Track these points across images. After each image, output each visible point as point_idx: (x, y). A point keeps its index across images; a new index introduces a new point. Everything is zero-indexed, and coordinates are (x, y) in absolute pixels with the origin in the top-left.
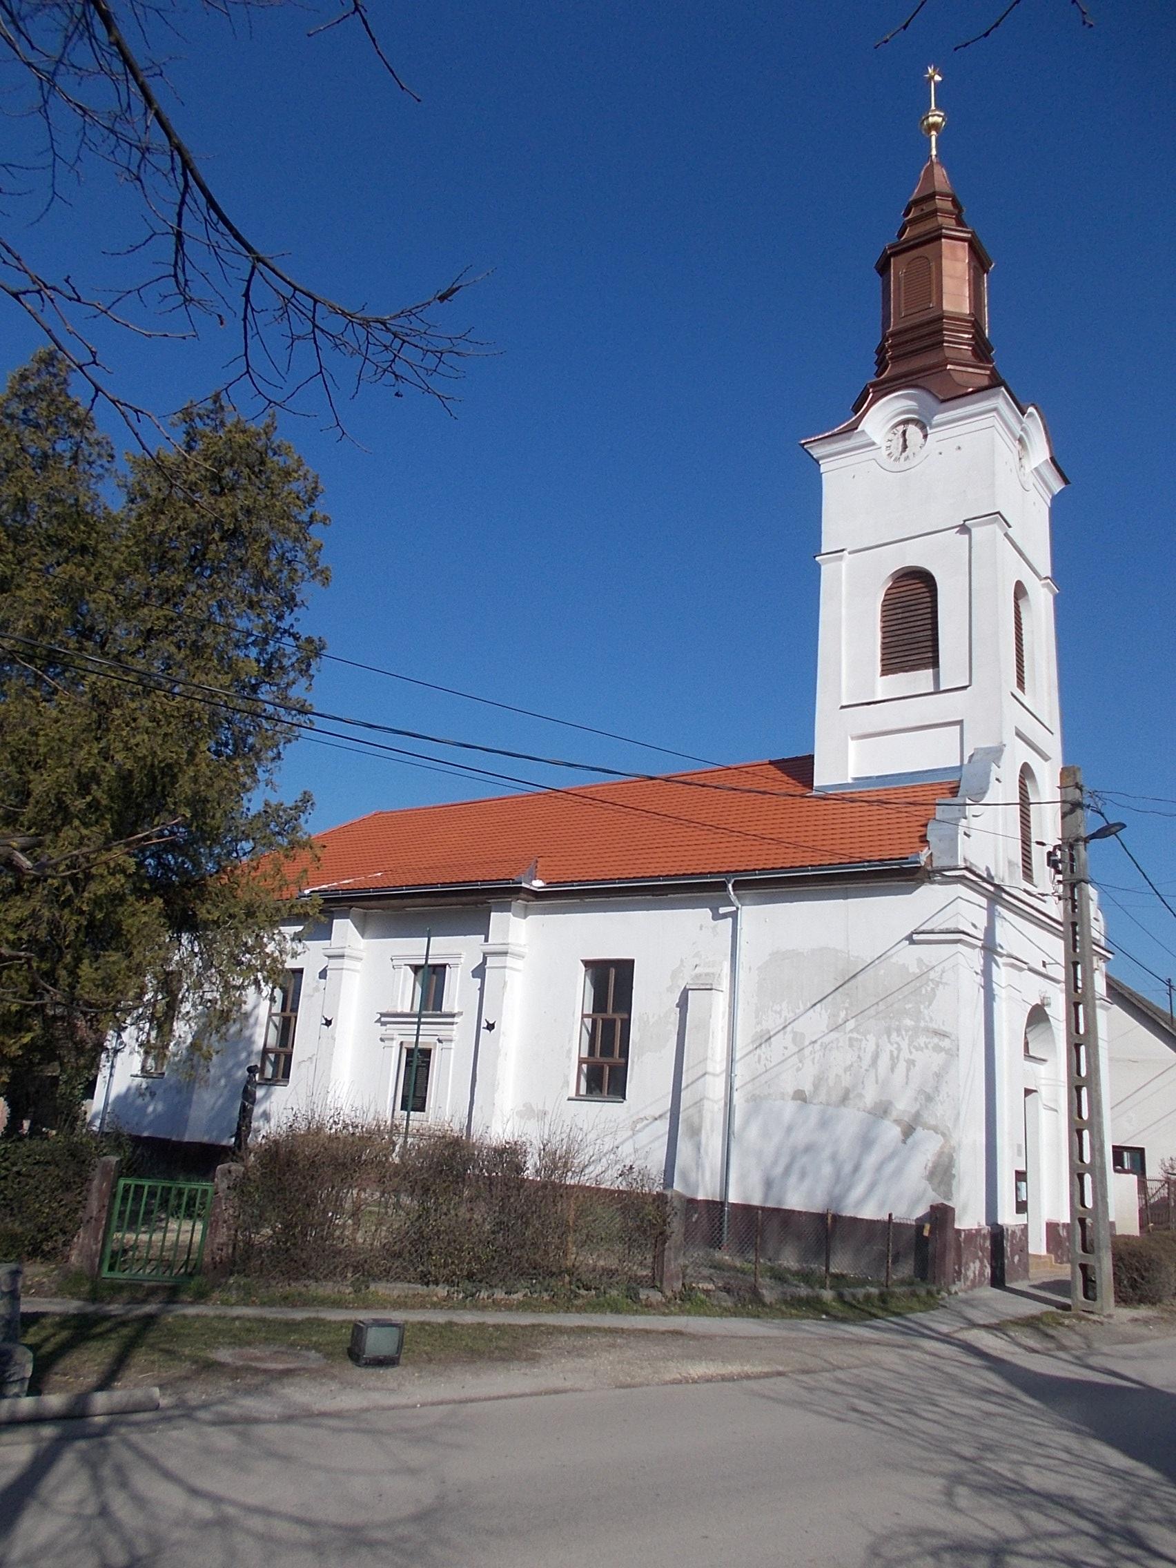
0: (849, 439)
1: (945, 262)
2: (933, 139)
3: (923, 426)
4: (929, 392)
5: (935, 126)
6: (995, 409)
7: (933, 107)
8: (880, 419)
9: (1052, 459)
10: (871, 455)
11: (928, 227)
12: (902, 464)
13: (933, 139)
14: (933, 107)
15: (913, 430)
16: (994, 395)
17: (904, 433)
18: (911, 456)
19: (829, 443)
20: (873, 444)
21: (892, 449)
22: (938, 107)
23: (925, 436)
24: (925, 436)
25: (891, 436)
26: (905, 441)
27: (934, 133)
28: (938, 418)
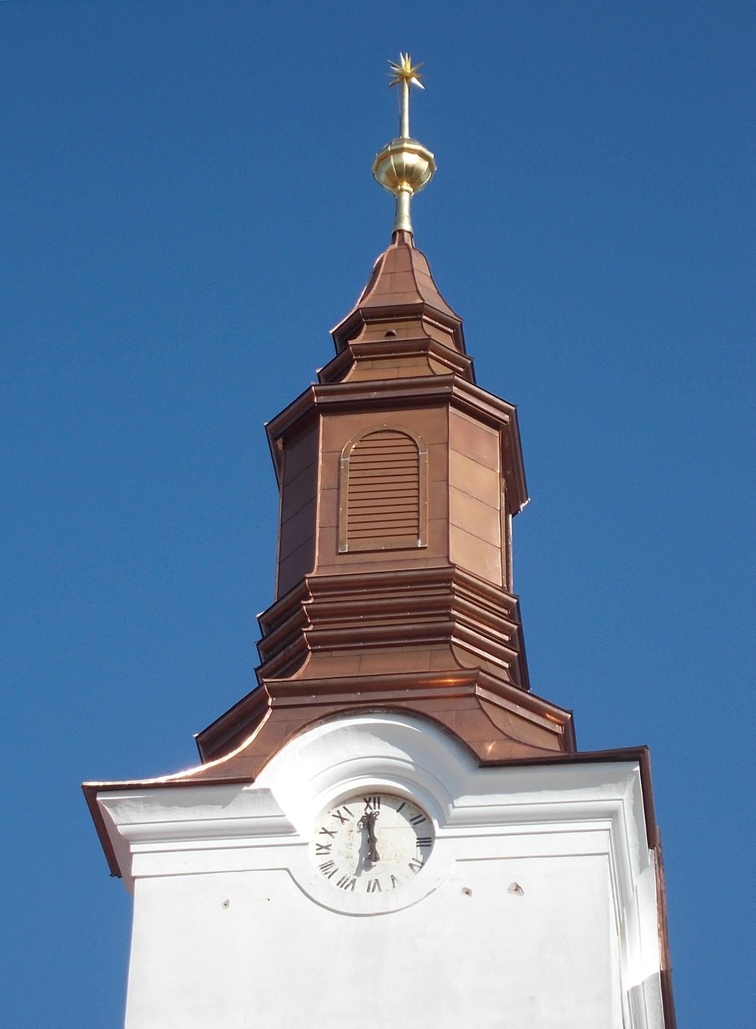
0: (224, 803)
1: (455, 459)
2: (406, 199)
3: (419, 818)
4: (449, 733)
5: (411, 174)
6: (612, 815)
7: (406, 134)
8: (315, 767)
9: (665, 976)
10: (281, 857)
11: (404, 373)
12: (359, 898)
13: (406, 199)
14: (406, 134)
15: (392, 824)
16: (615, 780)
17: (368, 822)
18: (385, 883)
19: (169, 804)
20: (288, 830)
21: (333, 856)
22: (414, 136)
23: (426, 842)
24: (426, 842)
25: (331, 823)
26: (370, 842)
27: (406, 186)
28: (465, 804)
